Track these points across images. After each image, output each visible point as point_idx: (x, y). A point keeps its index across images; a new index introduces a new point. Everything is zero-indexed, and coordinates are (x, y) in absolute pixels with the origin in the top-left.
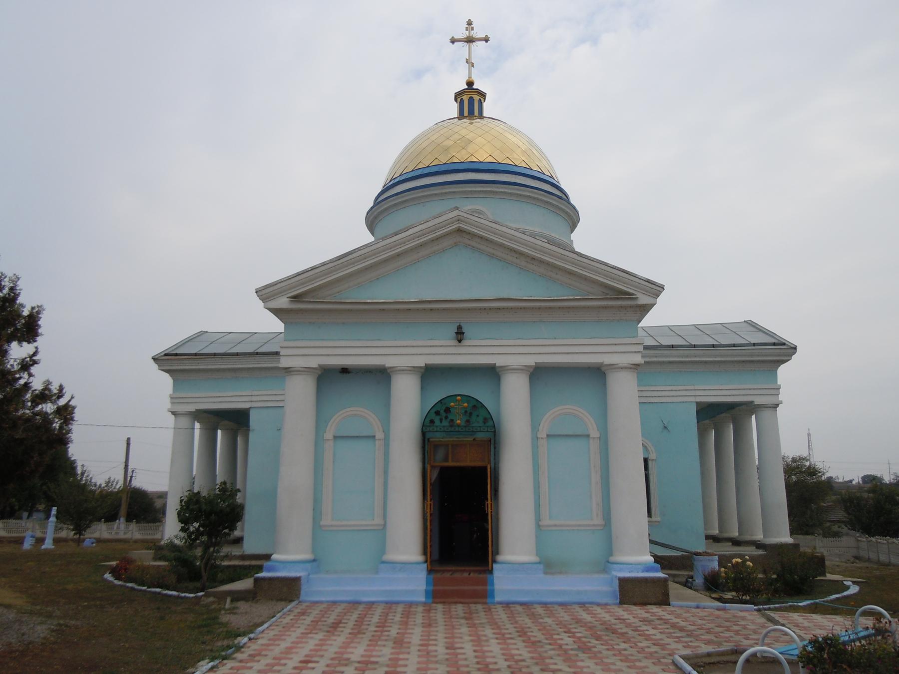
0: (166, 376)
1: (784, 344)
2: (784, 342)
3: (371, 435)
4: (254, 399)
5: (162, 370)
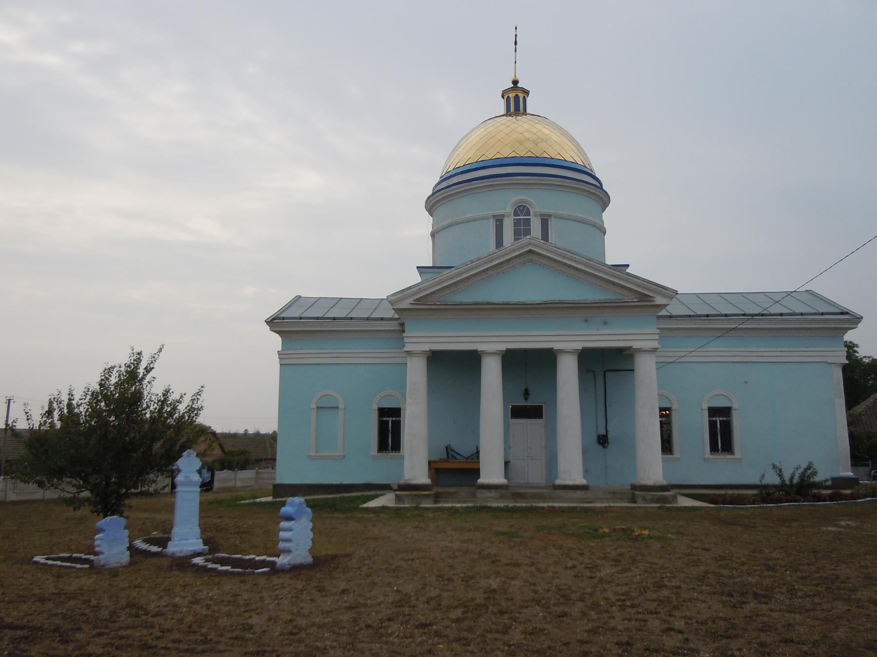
0: (277, 336)
1: (848, 313)
2: (847, 311)
5: (272, 331)
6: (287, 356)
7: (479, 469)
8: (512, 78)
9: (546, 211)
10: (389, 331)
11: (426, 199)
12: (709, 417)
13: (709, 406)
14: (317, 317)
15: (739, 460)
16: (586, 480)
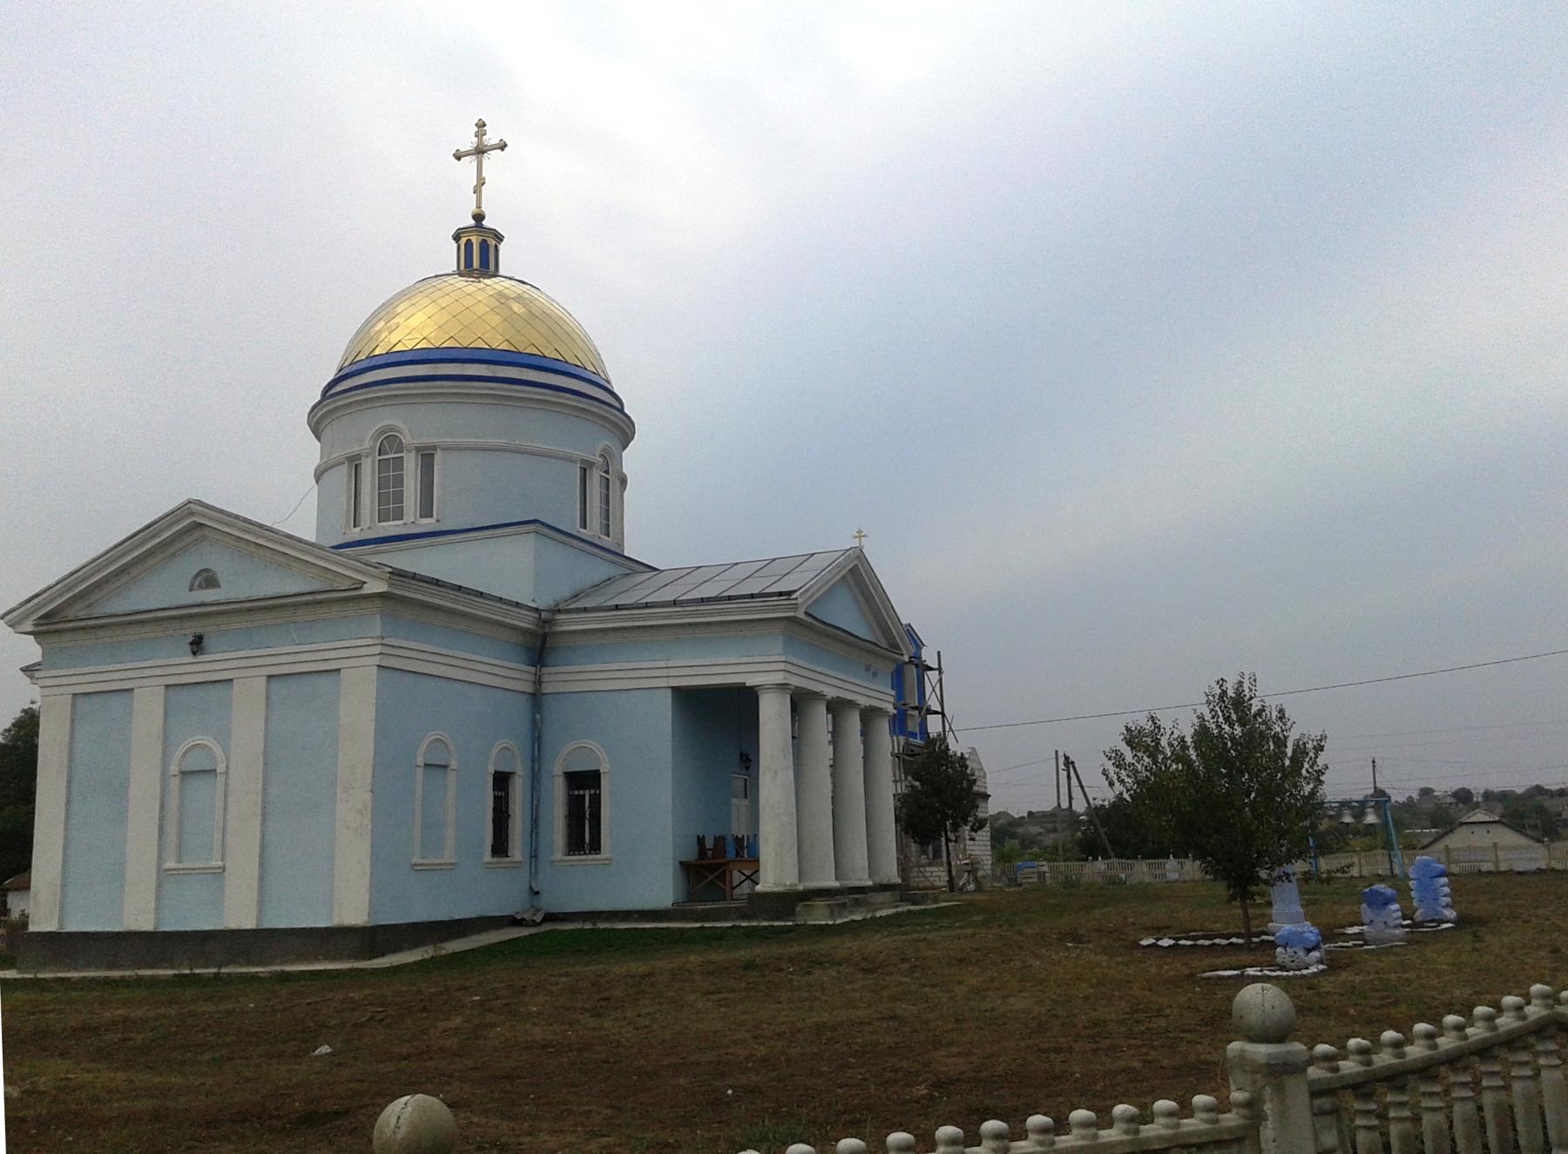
3: (207, 767)
6: (465, 664)
8: (473, 208)
9: (426, 440)
11: (308, 410)
13: (499, 769)
14: (780, 592)
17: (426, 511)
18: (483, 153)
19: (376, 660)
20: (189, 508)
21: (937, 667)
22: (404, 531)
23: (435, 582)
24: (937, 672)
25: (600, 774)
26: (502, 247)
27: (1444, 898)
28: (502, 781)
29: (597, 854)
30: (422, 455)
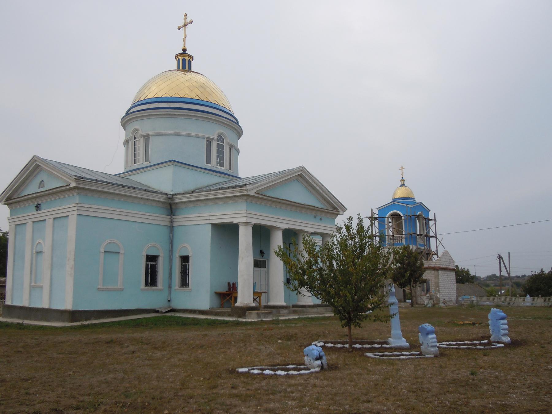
4: (211, 218)
6: (130, 215)
7: (237, 297)
8: (182, 47)
10: (156, 201)
12: (146, 262)
13: (147, 254)
15: (191, 290)
16: (285, 303)
17: (147, 159)
18: (186, 26)
19: (76, 212)
20: (303, 169)
21: (434, 219)
22: (140, 167)
23: (121, 185)
24: (434, 221)
25: (189, 257)
26: (193, 63)
27: (503, 331)
28: (152, 259)
29: (187, 287)
30: (146, 138)
